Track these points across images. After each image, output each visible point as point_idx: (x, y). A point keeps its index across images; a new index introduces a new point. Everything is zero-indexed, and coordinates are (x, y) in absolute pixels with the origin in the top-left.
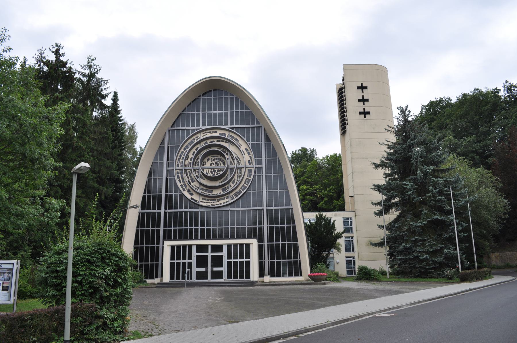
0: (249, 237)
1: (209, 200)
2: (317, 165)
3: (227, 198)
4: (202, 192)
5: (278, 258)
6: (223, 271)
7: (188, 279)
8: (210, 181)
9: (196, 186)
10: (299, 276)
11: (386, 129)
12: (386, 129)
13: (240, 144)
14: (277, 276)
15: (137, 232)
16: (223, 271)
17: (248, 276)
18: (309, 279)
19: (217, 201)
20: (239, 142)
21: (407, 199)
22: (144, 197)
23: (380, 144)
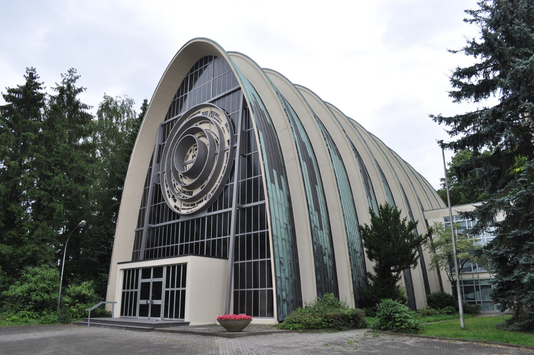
0: (186, 254)
1: (188, 206)
2: (142, 113)
3: (205, 200)
4: (184, 197)
5: (256, 286)
6: (160, 305)
7: (166, 316)
8: (191, 179)
9: (179, 189)
10: (258, 316)
11: (465, 20)
12: (465, 20)
13: (221, 120)
14: (260, 316)
15: (133, 253)
16: (160, 305)
17: (183, 316)
18: (218, 323)
19: (196, 205)
20: (220, 117)
21: (513, 150)
22: (140, 210)
23: (450, 51)
